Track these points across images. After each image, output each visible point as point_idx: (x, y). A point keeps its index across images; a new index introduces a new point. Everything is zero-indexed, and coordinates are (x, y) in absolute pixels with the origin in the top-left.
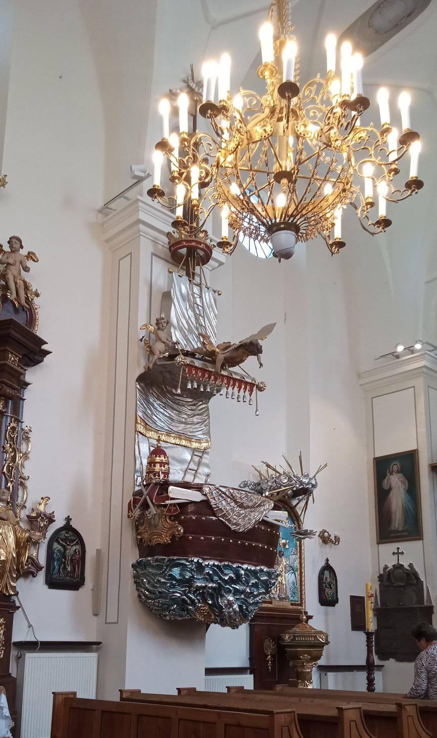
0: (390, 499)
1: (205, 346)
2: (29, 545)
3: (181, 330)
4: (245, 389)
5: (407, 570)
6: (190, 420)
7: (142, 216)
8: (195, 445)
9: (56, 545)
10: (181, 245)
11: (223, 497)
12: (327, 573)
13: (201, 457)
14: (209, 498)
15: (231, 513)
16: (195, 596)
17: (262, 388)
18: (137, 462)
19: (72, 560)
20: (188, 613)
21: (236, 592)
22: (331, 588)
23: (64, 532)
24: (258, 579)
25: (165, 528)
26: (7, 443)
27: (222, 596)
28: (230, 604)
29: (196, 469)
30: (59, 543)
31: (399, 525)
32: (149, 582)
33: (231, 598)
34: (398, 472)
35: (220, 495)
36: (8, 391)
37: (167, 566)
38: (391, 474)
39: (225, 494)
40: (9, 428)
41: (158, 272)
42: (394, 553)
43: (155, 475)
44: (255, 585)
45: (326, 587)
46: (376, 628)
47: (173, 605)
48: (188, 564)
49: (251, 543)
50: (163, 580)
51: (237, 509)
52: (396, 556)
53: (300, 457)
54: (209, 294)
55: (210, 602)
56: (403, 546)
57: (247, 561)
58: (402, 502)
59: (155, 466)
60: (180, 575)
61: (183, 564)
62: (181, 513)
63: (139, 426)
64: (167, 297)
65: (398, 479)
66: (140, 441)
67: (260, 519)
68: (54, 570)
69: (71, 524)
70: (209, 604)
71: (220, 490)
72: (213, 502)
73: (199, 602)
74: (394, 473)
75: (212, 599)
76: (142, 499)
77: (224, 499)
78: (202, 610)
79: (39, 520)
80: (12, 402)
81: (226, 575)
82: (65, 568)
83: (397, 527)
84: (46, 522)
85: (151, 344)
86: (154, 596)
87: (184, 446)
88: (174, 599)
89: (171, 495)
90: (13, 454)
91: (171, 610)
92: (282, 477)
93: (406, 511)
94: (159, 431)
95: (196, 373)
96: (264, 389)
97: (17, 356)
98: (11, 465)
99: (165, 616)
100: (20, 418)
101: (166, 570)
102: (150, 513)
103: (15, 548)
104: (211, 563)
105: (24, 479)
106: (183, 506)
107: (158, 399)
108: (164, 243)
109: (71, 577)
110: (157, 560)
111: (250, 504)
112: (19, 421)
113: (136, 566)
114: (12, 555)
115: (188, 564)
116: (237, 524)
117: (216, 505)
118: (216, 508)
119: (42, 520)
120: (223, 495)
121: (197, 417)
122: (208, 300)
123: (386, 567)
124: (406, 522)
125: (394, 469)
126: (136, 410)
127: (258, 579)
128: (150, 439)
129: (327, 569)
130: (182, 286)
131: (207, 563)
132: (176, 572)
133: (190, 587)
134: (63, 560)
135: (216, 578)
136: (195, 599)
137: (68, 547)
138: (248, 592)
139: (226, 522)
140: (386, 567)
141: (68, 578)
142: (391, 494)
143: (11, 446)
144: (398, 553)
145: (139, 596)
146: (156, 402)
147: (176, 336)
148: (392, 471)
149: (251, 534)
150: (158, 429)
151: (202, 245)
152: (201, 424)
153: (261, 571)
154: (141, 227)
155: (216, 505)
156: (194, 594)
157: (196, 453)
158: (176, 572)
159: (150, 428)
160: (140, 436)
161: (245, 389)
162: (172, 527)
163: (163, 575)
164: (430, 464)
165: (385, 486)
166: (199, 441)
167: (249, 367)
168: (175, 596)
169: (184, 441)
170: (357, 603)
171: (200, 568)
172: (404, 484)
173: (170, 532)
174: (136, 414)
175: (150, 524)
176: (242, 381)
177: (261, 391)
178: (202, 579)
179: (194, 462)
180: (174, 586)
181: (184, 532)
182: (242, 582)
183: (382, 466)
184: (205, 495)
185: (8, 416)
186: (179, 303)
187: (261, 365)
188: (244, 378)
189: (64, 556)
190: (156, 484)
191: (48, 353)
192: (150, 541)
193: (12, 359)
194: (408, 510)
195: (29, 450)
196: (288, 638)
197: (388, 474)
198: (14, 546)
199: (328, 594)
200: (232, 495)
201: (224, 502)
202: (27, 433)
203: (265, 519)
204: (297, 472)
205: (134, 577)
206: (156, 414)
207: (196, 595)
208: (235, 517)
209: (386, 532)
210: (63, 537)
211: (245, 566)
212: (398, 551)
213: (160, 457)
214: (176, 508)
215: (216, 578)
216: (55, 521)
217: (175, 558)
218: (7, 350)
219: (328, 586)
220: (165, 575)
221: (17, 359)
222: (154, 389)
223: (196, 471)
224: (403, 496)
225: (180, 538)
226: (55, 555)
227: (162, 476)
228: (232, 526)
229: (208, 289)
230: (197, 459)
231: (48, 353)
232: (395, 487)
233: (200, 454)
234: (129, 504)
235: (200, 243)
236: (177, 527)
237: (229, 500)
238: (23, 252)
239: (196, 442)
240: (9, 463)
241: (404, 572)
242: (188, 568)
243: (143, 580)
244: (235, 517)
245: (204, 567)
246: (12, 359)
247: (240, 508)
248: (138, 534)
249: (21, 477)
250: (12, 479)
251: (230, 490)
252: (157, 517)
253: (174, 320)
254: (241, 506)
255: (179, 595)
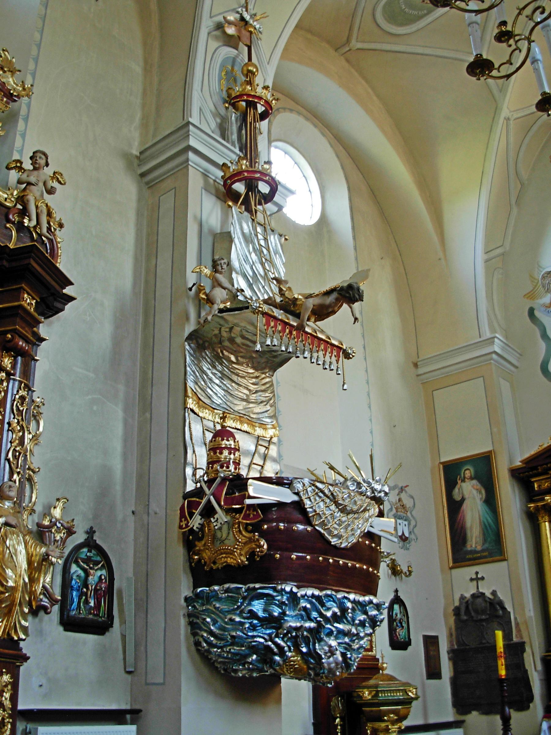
0: (463, 511)
1: (282, 292)
2: (45, 566)
3: (245, 276)
4: (332, 352)
5: (489, 598)
6: (253, 397)
7: (193, 142)
8: (259, 431)
9: (74, 568)
10: (242, 176)
11: (320, 497)
12: (396, 607)
13: (267, 448)
14: (303, 498)
15: (331, 521)
16: (284, 641)
17: (349, 354)
18: (188, 451)
19: (96, 590)
20: (271, 667)
21: (341, 633)
22: (403, 627)
23: (85, 550)
24: (366, 613)
25: (239, 542)
26: (14, 418)
27: (320, 640)
28: (332, 652)
29: (261, 464)
30: (79, 566)
31: (476, 543)
32: (215, 622)
33: (333, 643)
34: (471, 478)
35: (317, 494)
36: (21, 343)
37: (244, 598)
38: (463, 481)
39: (322, 491)
40: (17, 397)
41: (206, 210)
42: (472, 580)
43: (222, 467)
44: (362, 624)
45: (397, 625)
46: (452, 674)
47: (251, 655)
48: (275, 594)
49: (347, 562)
50: (238, 619)
51: (338, 515)
52: (475, 582)
53: (371, 457)
54: (274, 238)
55: (304, 650)
56: (483, 570)
57: (346, 588)
58: (479, 516)
59: (221, 453)
60: (265, 610)
61: (268, 595)
62: (264, 521)
63: (190, 401)
64: (225, 239)
65: (473, 486)
66: (191, 422)
67: (365, 530)
68: (72, 605)
69: (94, 538)
70: (301, 651)
71: (316, 487)
72: (307, 503)
73: (290, 650)
74: (466, 480)
75: (307, 645)
76: (204, 501)
77: (323, 500)
78: (292, 661)
79: (53, 530)
80: (22, 361)
81: (328, 609)
82: (87, 602)
83: (474, 546)
84: (64, 534)
85: (208, 292)
86: (222, 642)
87: (246, 432)
88: (254, 646)
89: (252, 494)
90: (21, 434)
91: (248, 663)
92: (349, 483)
93: (485, 528)
94: (214, 409)
95: (275, 326)
96: (353, 356)
97: (33, 298)
98: (18, 449)
99: (236, 671)
100: (31, 385)
101: (242, 604)
102: (217, 521)
103: (26, 569)
104: (310, 592)
105: (34, 472)
106: (266, 508)
107: (214, 367)
108: (216, 178)
109: (94, 615)
110: (227, 591)
111: (355, 508)
112: (30, 389)
113: (192, 599)
114: (23, 579)
115: (275, 594)
116: (339, 537)
117: (311, 507)
118: (312, 512)
119: (58, 531)
120: (321, 494)
121: (260, 393)
122: (274, 245)
123: (462, 598)
124: (485, 541)
125: (466, 476)
126: (185, 379)
127: (366, 613)
128: (204, 420)
129: (397, 603)
130: (240, 225)
131: (303, 593)
132: (258, 606)
133: (277, 629)
134: (85, 590)
135: (314, 614)
136: (285, 645)
137: (92, 571)
138: (353, 633)
139: (325, 533)
140: (462, 598)
141: (91, 616)
142: (464, 506)
143: (18, 422)
144: (477, 579)
145: (197, 644)
146: (210, 369)
147: (240, 283)
148: (464, 477)
149: (353, 552)
150: (214, 407)
151: (267, 178)
152: (265, 403)
153: (371, 602)
154: (191, 155)
155: (311, 507)
156: (283, 639)
157: (260, 442)
158: (258, 606)
159: (204, 405)
160: (192, 414)
161: (332, 352)
162: (251, 540)
163: (238, 612)
164: (510, 468)
165: (457, 496)
166: (263, 426)
167: (337, 326)
168: (256, 641)
169: (245, 425)
170: (431, 642)
171: (294, 598)
172: (480, 492)
173: (246, 549)
174: (186, 384)
175: (214, 537)
176: (327, 342)
177: (348, 359)
178: (296, 616)
179: (259, 454)
180: (253, 628)
181: (269, 549)
182: (346, 619)
183: (451, 472)
184: (297, 494)
185: (14, 380)
186: (240, 243)
187: (356, 319)
188: (330, 339)
189: (86, 585)
190: (224, 479)
191: (71, 299)
192: (214, 563)
193: (28, 301)
194: (488, 526)
195: (41, 429)
196: (369, 695)
197: (459, 482)
198: (26, 566)
199: (399, 635)
200: (332, 494)
201: (321, 504)
202: (38, 407)
203: (371, 530)
204: (366, 474)
205: (189, 615)
206: (210, 386)
207: (286, 639)
208: (336, 526)
209: (461, 553)
210: (83, 556)
211: (352, 596)
212: (477, 576)
213: (228, 440)
214: (257, 512)
215: (314, 614)
216: (75, 533)
217: (257, 586)
218: (22, 288)
219: (399, 625)
220: (242, 612)
221: (34, 302)
222: (207, 353)
223: (262, 467)
224: (480, 508)
225: (262, 557)
226: (73, 582)
227: (232, 467)
228: (332, 539)
229: (273, 231)
230: (262, 450)
231: (71, 299)
232: (469, 498)
233: (267, 445)
234: (182, 509)
235: (266, 175)
236: (258, 540)
237: (328, 501)
238: (49, 171)
239: (259, 427)
240: (16, 447)
241: (486, 601)
242: (276, 600)
243: (205, 619)
244: (336, 526)
245: (299, 598)
246: (28, 301)
247: (342, 512)
248: (531, 500)
249: (29, 469)
250: (18, 470)
251: (330, 487)
252: (225, 527)
253: (235, 263)
254: (344, 510)
255: (262, 640)
